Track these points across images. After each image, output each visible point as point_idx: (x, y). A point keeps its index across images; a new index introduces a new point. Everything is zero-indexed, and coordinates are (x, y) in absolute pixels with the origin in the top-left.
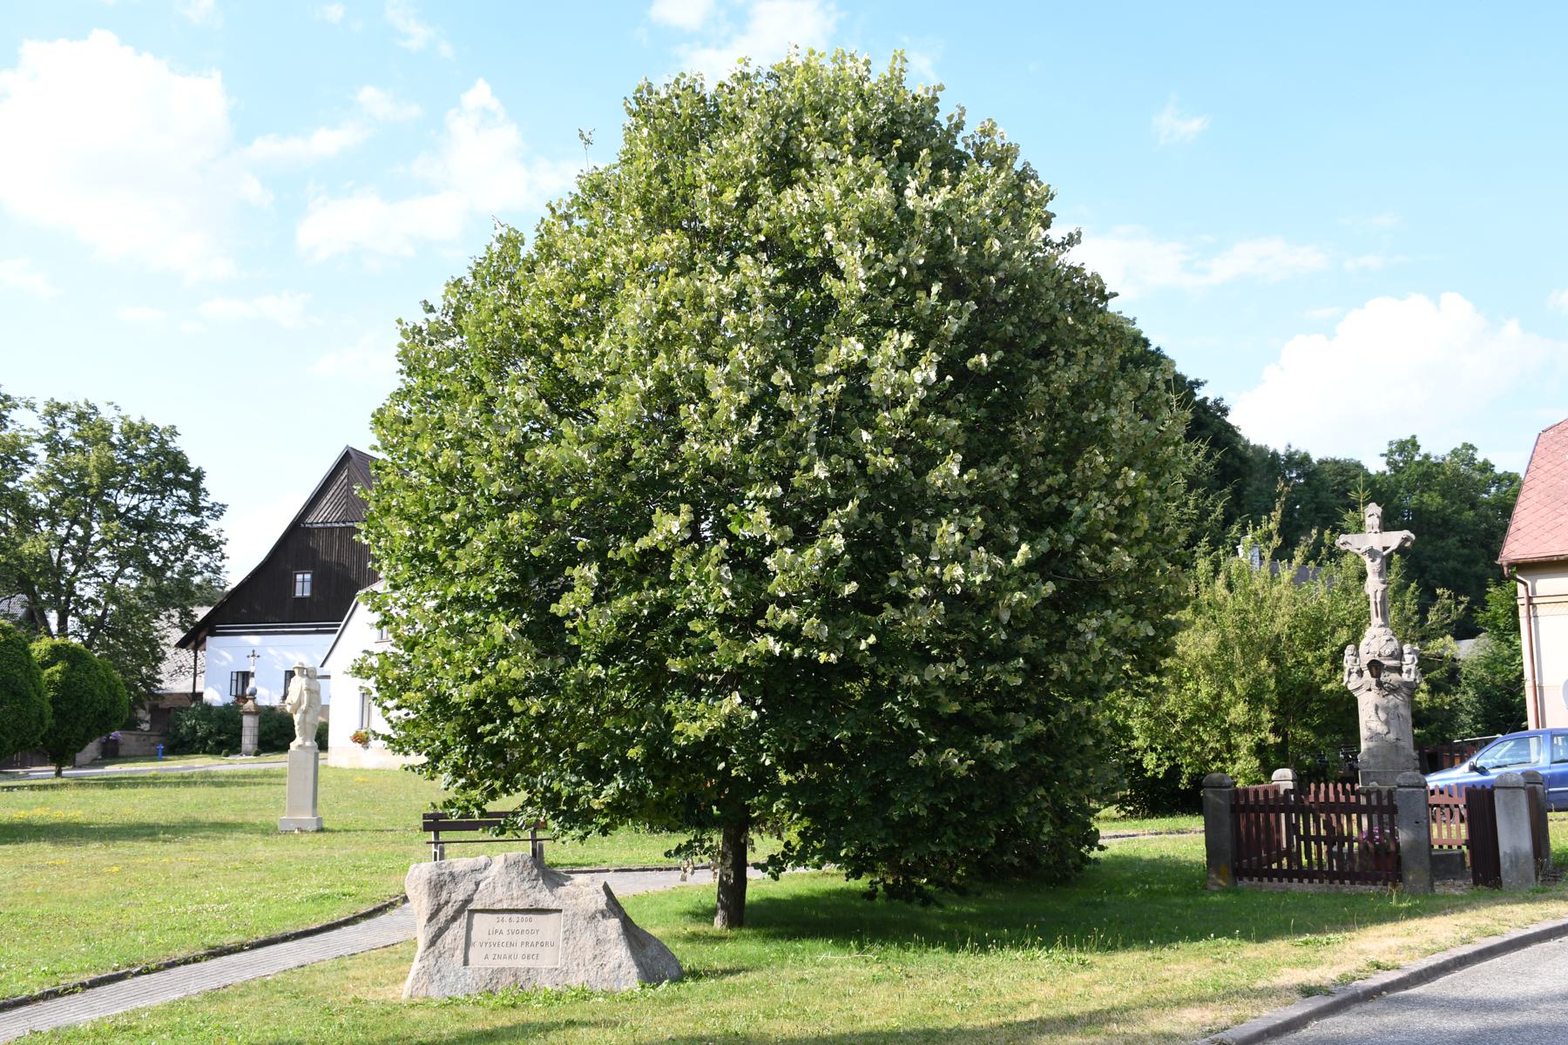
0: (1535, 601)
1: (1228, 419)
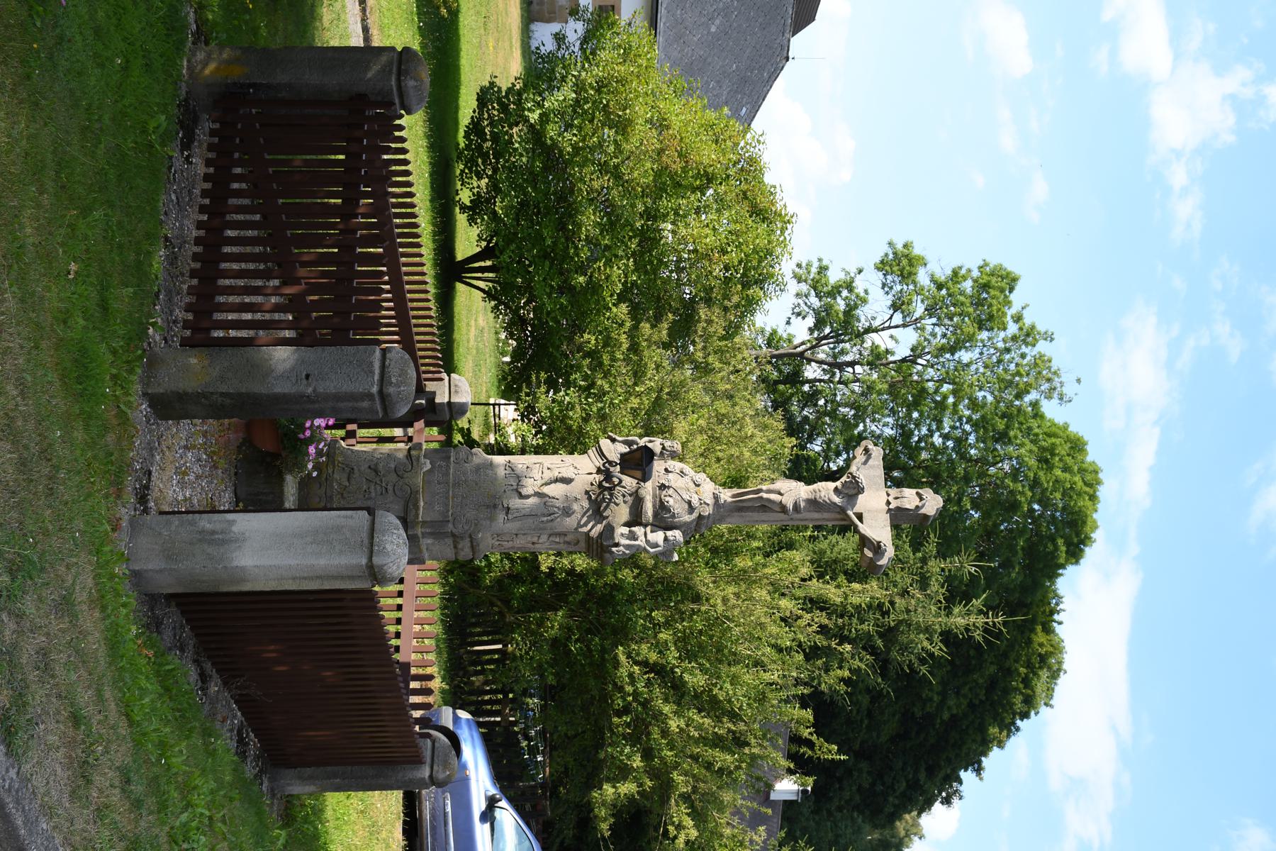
1: (937, 806)
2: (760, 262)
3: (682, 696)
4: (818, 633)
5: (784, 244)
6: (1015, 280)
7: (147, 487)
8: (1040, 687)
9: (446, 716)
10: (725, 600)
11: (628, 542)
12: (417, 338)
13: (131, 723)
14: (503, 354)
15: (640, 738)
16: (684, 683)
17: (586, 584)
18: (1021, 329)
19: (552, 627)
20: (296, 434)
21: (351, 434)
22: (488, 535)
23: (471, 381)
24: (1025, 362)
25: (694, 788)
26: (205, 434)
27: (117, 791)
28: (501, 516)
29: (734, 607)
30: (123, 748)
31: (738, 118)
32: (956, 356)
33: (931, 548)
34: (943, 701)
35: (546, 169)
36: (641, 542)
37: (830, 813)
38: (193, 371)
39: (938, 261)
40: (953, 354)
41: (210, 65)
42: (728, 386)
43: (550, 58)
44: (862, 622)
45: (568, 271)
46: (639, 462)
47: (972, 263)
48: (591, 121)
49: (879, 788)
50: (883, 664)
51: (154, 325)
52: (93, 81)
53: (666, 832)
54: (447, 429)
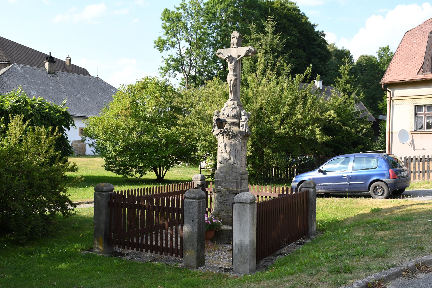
0: (393, 99)
2: (159, 86)
3: (290, 114)
4: (273, 72)
5: (154, 79)
6: (166, 10)
7: (224, 269)
8: (290, 6)
9: (294, 184)
10: (262, 100)
11: (245, 127)
12: (181, 189)
13: (295, 273)
14: (185, 166)
15: (303, 127)
16: (287, 113)
17: (256, 142)
18: (182, 8)
19: (269, 152)
20: (209, 226)
21: (209, 210)
22: (241, 169)
23: (194, 175)
24: (191, 7)
25: (318, 111)
26: (209, 252)
27: (315, 277)
28: (236, 165)
29: (264, 97)
30: (302, 275)
31: (115, 92)
32: (189, 28)
33: (247, 37)
34: (294, 36)
35: (130, 150)
36: (245, 123)
37: (326, 71)
38: (190, 254)
39: (159, 33)
40: (188, 29)
41: (99, 247)
42: (197, 97)
43: (97, 148)
44: (269, 59)
45: (161, 144)
46: (220, 123)
47: (161, 23)
48: (116, 136)
49: (319, 56)
50: (282, 53)
51: (176, 265)
52: (104, 280)
53: (331, 120)
54: (208, 183)
